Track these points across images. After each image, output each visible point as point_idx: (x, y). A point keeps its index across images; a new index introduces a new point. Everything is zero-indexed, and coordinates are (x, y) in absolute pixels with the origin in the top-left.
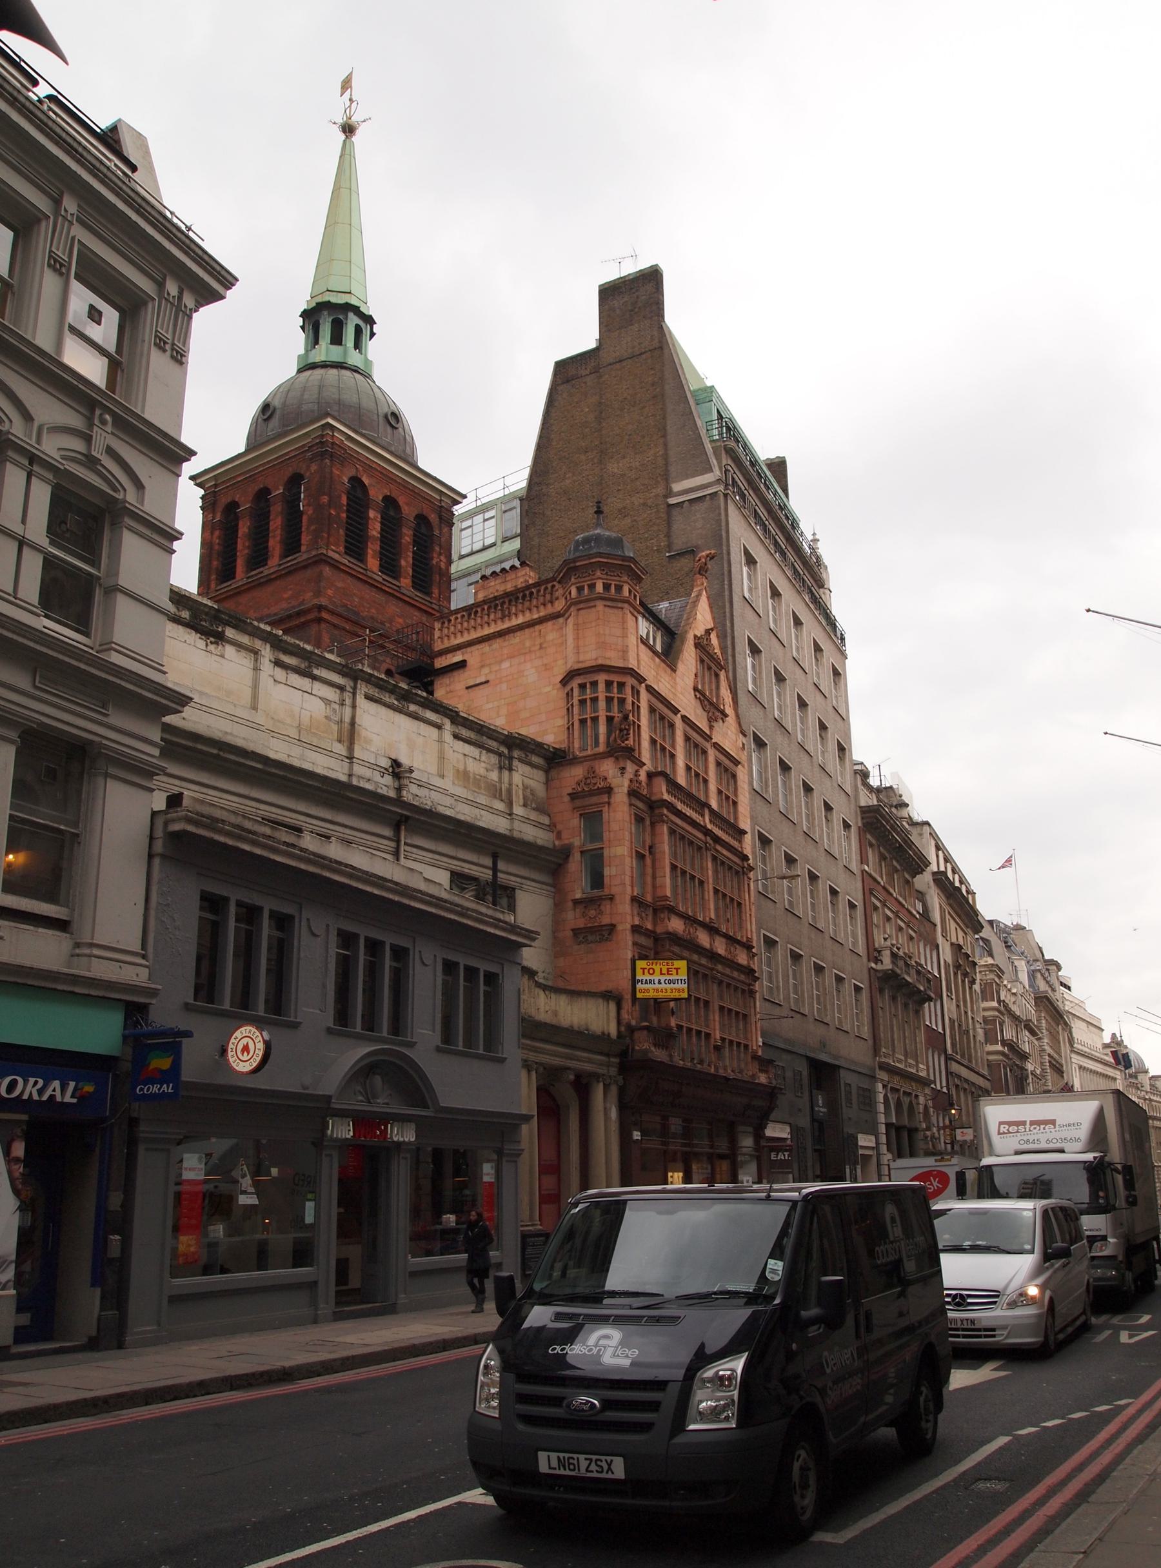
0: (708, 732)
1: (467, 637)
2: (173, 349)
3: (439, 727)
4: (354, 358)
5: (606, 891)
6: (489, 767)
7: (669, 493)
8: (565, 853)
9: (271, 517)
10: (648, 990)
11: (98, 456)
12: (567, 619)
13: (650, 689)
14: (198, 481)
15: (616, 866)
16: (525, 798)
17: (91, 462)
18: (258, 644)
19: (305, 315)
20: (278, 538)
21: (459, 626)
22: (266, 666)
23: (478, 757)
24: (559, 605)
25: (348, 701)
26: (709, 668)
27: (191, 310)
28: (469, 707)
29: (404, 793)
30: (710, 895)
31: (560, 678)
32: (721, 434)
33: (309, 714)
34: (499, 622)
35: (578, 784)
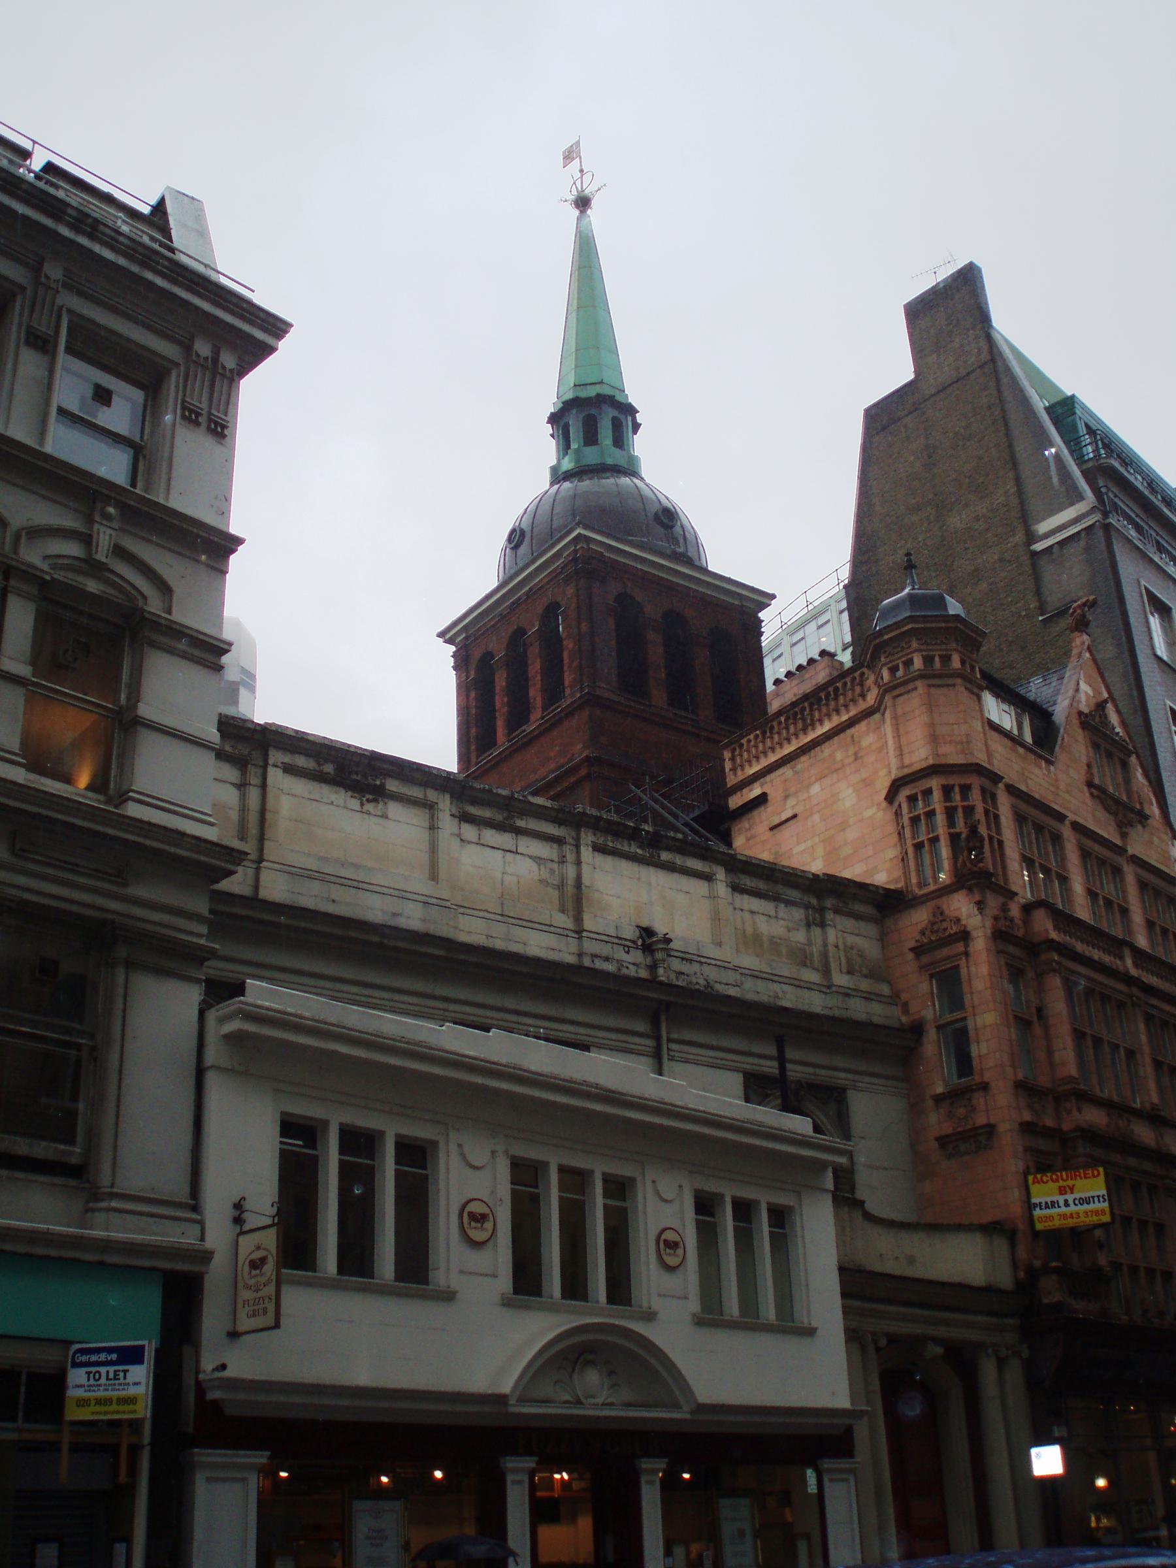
0: (1118, 842)
1: (764, 763)
2: (210, 421)
3: (708, 878)
4: (614, 456)
5: (977, 1078)
6: (790, 925)
7: (1031, 538)
8: (917, 1029)
9: (530, 662)
10: (1051, 1218)
11: (103, 559)
12: (883, 715)
13: (1012, 790)
14: (447, 637)
15: (987, 1041)
16: (849, 960)
17: (93, 567)
18: (432, 795)
19: (554, 419)
20: (538, 686)
21: (754, 750)
22: (447, 824)
23: (773, 913)
24: (871, 699)
25: (570, 857)
26: (1109, 755)
27: (231, 371)
28: (776, 853)
29: (661, 971)
30: (1147, 1069)
31: (884, 793)
32: (1096, 450)
33: (514, 879)
34: (801, 735)
35: (922, 933)
